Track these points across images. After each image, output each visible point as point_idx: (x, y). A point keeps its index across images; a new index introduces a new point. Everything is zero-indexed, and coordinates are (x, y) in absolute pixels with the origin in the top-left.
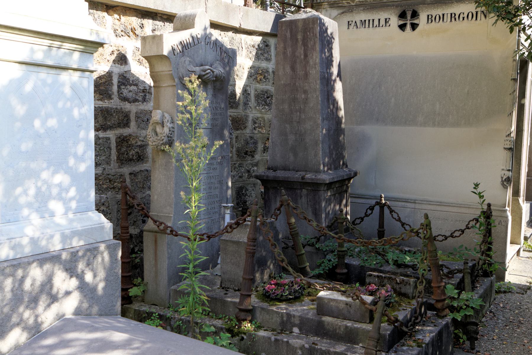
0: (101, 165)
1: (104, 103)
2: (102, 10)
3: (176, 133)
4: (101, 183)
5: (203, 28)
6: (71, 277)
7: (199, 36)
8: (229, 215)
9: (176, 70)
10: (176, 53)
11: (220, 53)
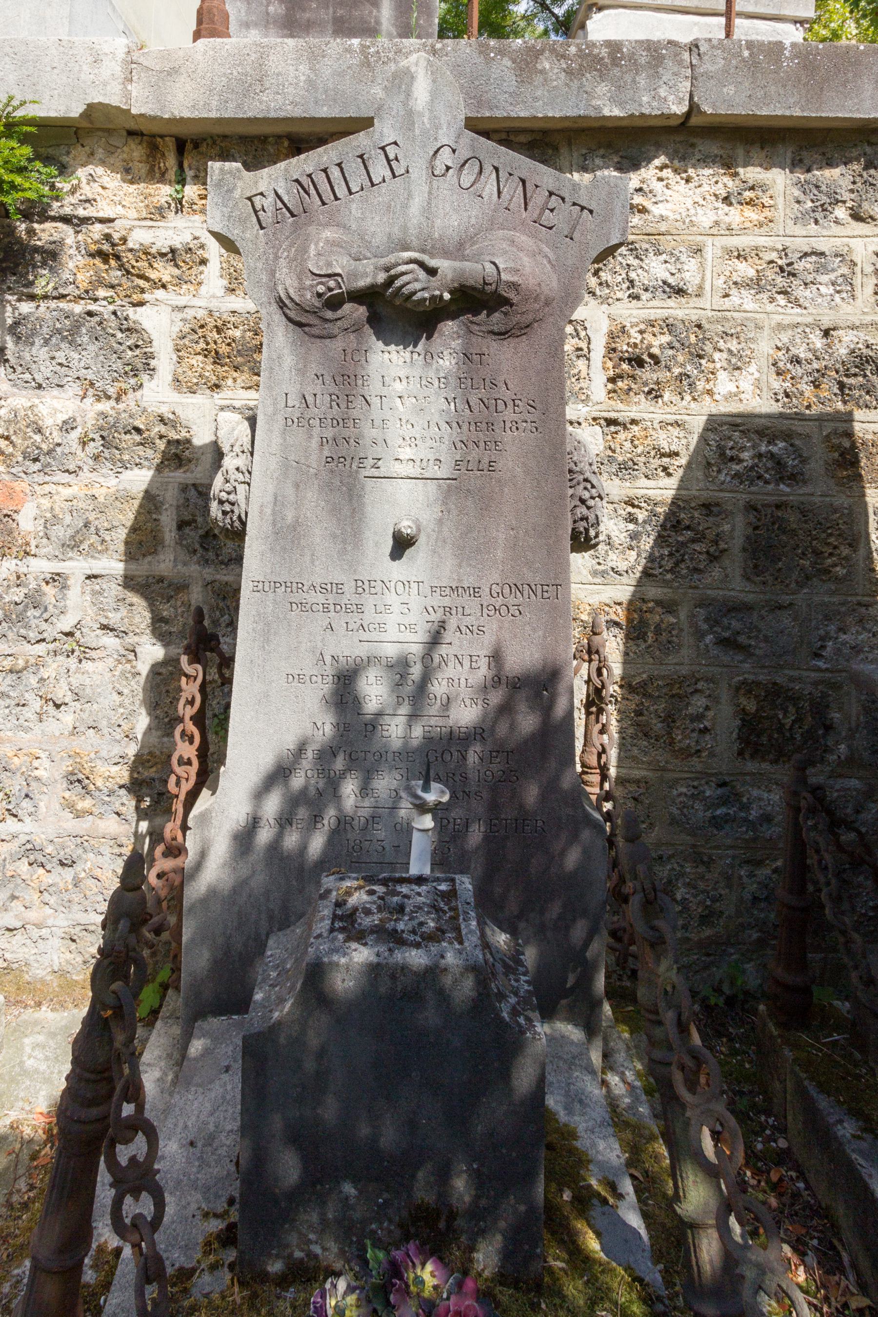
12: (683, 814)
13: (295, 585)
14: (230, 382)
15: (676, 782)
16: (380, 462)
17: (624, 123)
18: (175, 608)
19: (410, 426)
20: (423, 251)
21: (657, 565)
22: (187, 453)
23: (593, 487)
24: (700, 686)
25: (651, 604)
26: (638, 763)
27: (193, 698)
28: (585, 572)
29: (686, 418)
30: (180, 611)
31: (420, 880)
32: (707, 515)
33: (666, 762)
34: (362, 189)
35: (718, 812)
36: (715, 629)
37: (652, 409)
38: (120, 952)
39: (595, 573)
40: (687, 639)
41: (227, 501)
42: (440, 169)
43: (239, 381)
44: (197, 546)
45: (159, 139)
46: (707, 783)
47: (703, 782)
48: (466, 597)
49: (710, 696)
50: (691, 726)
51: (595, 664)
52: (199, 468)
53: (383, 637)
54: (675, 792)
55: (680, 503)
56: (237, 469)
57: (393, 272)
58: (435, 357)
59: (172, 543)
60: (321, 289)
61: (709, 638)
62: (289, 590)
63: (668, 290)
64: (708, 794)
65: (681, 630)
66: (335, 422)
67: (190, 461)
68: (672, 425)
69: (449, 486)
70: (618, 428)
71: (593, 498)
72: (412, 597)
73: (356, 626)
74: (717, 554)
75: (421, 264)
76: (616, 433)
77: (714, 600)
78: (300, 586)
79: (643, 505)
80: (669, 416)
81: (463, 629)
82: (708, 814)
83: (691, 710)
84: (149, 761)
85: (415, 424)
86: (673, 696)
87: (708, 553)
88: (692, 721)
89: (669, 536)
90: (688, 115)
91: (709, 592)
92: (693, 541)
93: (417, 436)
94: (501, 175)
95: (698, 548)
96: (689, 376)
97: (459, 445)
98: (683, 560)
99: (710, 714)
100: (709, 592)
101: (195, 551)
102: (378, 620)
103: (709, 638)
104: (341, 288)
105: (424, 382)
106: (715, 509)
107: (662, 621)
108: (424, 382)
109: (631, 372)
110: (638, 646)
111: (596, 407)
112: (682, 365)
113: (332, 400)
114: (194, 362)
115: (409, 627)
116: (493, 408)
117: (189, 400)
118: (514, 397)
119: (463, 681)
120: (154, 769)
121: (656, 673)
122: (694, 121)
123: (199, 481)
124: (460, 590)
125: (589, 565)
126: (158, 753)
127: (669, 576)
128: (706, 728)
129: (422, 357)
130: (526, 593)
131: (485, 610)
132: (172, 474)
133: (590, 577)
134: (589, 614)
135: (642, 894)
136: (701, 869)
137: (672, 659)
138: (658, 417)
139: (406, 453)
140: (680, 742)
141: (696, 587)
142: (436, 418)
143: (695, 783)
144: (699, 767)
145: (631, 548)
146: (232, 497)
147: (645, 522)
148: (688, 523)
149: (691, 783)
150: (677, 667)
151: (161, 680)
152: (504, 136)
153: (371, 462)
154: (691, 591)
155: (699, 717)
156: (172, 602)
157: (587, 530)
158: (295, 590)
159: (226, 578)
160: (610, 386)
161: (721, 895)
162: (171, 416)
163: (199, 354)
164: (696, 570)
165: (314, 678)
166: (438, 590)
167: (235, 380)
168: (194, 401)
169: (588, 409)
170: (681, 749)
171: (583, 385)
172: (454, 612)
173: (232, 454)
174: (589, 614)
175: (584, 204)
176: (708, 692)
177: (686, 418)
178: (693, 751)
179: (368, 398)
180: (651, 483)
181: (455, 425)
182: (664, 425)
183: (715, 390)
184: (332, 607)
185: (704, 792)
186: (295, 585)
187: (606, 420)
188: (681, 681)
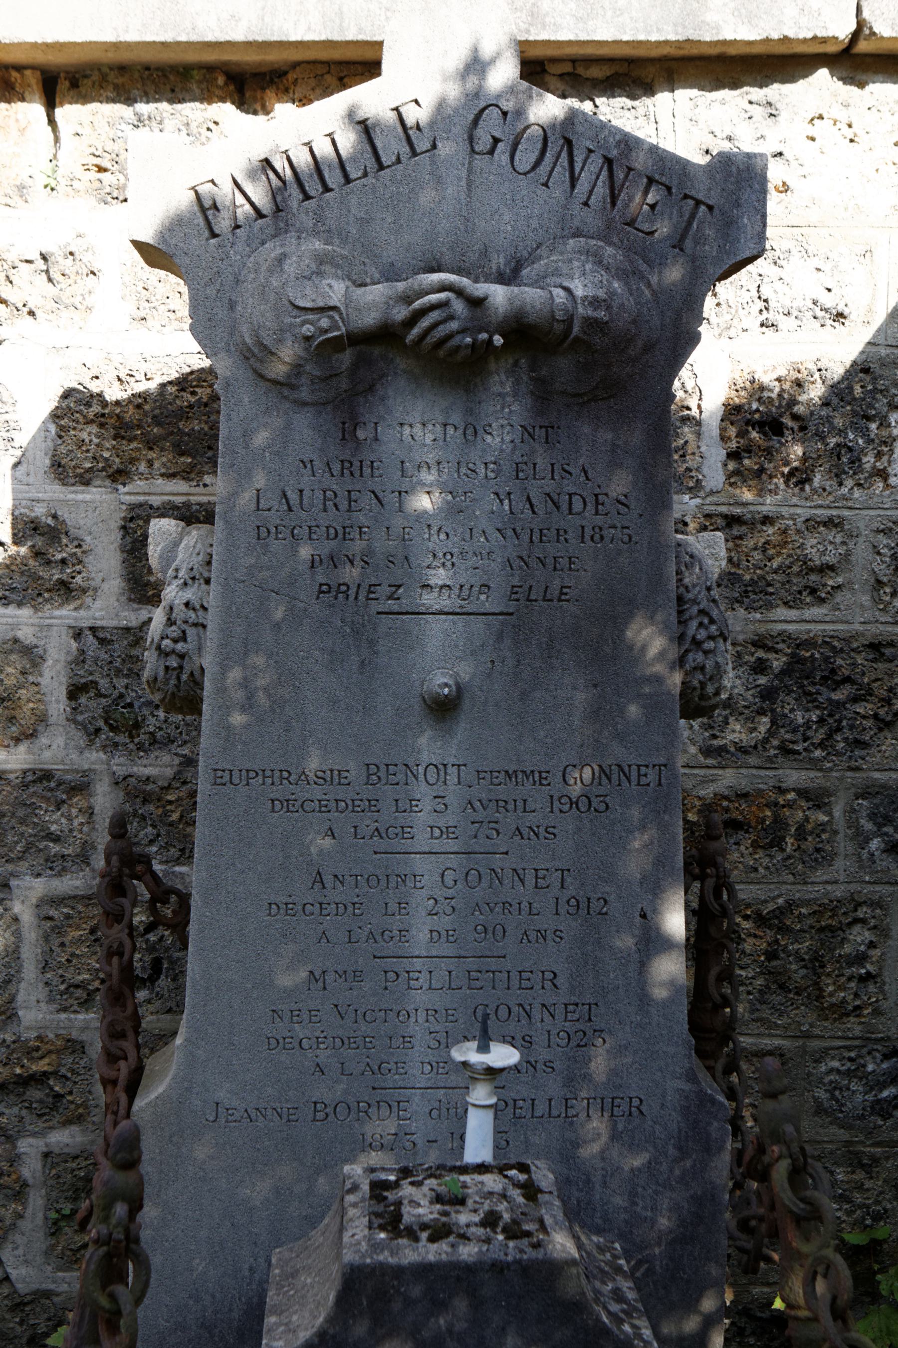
0: (173, 747)
1: (201, 489)
2: (207, 97)
3: (212, 636)
4: (175, 816)
5: (457, 58)
6: (18, 1156)
7: (412, 115)
8: (489, 1115)
9: (222, 313)
10: (223, 224)
11: (602, 190)
12: (833, 1097)
13: (277, 774)
14: (143, 467)
15: (825, 1053)
16: (401, 591)
17: (756, 50)
18: (70, 819)
19: (443, 536)
20: (458, 271)
21: (799, 736)
22: (79, 579)
23: (712, 621)
24: (860, 914)
25: (791, 796)
26: (770, 1028)
27: (121, 944)
28: (693, 750)
29: (846, 513)
30: (76, 823)
31: (482, 1168)
32: (874, 660)
33: (811, 1025)
34: (365, 175)
35: (885, 1094)
36: (885, 829)
37: (795, 500)
38: (119, 1241)
39: (707, 752)
40: (843, 844)
41: (173, 651)
42: (483, 142)
43: (157, 465)
44: (101, 723)
45: (14, 74)
46: (869, 1053)
47: (864, 1051)
48: (528, 785)
49: (875, 927)
50: (848, 972)
51: (710, 882)
52: (98, 604)
53: (407, 845)
54: (823, 1068)
55: (836, 643)
56: (187, 604)
57: (417, 304)
58: (481, 432)
59: (62, 720)
60: (308, 330)
61: (875, 844)
62: (269, 781)
63: (820, 314)
64: (870, 1068)
65: (836, 832)
66: (332, 531)
67: (84, 591)
68: (825, 524)
69: (502, 623)
70: (744, 529)
71: (711, 638)
72: (451, 788)
73: (368, 832)
74: (889, 718)
75: (459, 292)
76: (740, 538)
77: (884, 787)
78: (285, 774)
79: (781, 646)
80: (819, 512)
81: (525, 831)
82: (870, 1097)
83: (847, 949)
84: (37, 1049)
85: (451, 533)
86: (822, 930)
87: (876, 716)
88: (850, 964)
89: (818, 693)
90: (856, 35)
91: (877, 775)
92: (855, 700)
93: (455, 550)
94: (576, 152)
95: (861, 711)
96: (850, 449)
97: (517, 563)
98: (839, 729)
99: (876, 953)
100: (877, 775)
101: (98, 731)
102: (401, 822)
103: (875, 844)
104: (339, 329)
105: (463, 470)
106: (888, 651)
107: (807, 819)
108: (463, 470)
109: (764, 444)
110: (771, 857)
111: (709, 500)
112: (841, 432)
113: (325, 499)
114: (84, 435)
115: (446, 831)
116: (565, 507)
117: (80, 497)
118: (597, 491)
119: (525, 905)
120: (46, 1060)
121: (797, 895)
122: (863, 46)
123: (99, 623)
124: (520, 776)
125: (699, 739)
126: (51, 1036)
127: (818, 753)
128: (868, 973)
129: (460, 431)
130: (615, 777)
131: (556, 804)
132: (57, 613)
133: (702, 759)
134: (700, 812)
135: (789, 1161)
136: (860, 1175)
137: (820, 875)
138: (803, 513)
139: (440, 576)
140: (831, 995)
141: (858, 769)
142: (484, 523)
143: (853, 1054)
144: (858, 1030)
145: (761, 712)
146: (180, 646)
147: (783, 672)
148: (847, 673)
149: (847, 1054)
150: (829, 887)
151: (53, 929)
152: (567, 68)
153: (384, 590)
154: (849, 774)
155: (861, 959)
156: (65, 808)
157: (703, 685)
158: (277, 780)
159: (148, 771)
160: (731, 466)
161: (886, 1210)
162: (50, 521)
163: (92, 422)
164: (859, 743)
165: (308, 907)
166: (488, 776)
167: (150, 463)
168: (88, 497)
169: (698, 501)
170: (833, 1005)
171: (690, 464)
172: (511, 806)
173: (176, 583)
174: (700, 812)
175: (701, 196)
176: (873, 922)
177: (846, 513)
178: (850, 1008)
179: (380, 495)
180: (793, 614)
181: (510, 533)
182: (812, 524)
183: (889, 470)
184: (333, 804)
185: (864, 1066)
186: (277, 774)
187: (725, 517)
188: (832, 907)
